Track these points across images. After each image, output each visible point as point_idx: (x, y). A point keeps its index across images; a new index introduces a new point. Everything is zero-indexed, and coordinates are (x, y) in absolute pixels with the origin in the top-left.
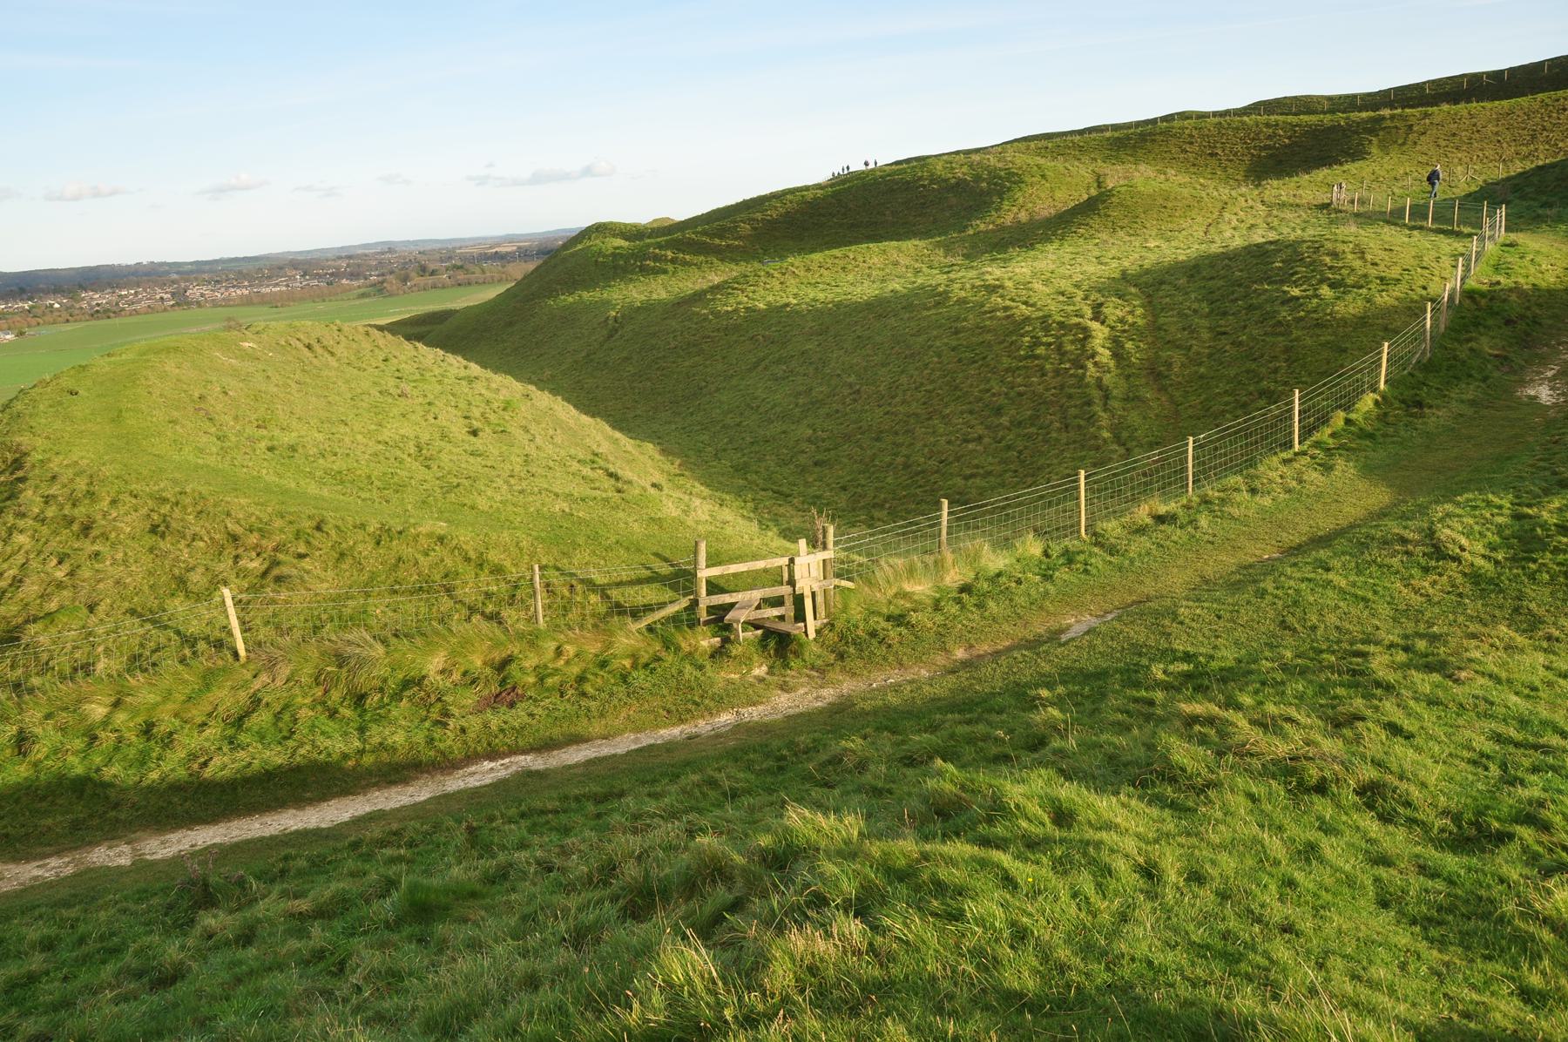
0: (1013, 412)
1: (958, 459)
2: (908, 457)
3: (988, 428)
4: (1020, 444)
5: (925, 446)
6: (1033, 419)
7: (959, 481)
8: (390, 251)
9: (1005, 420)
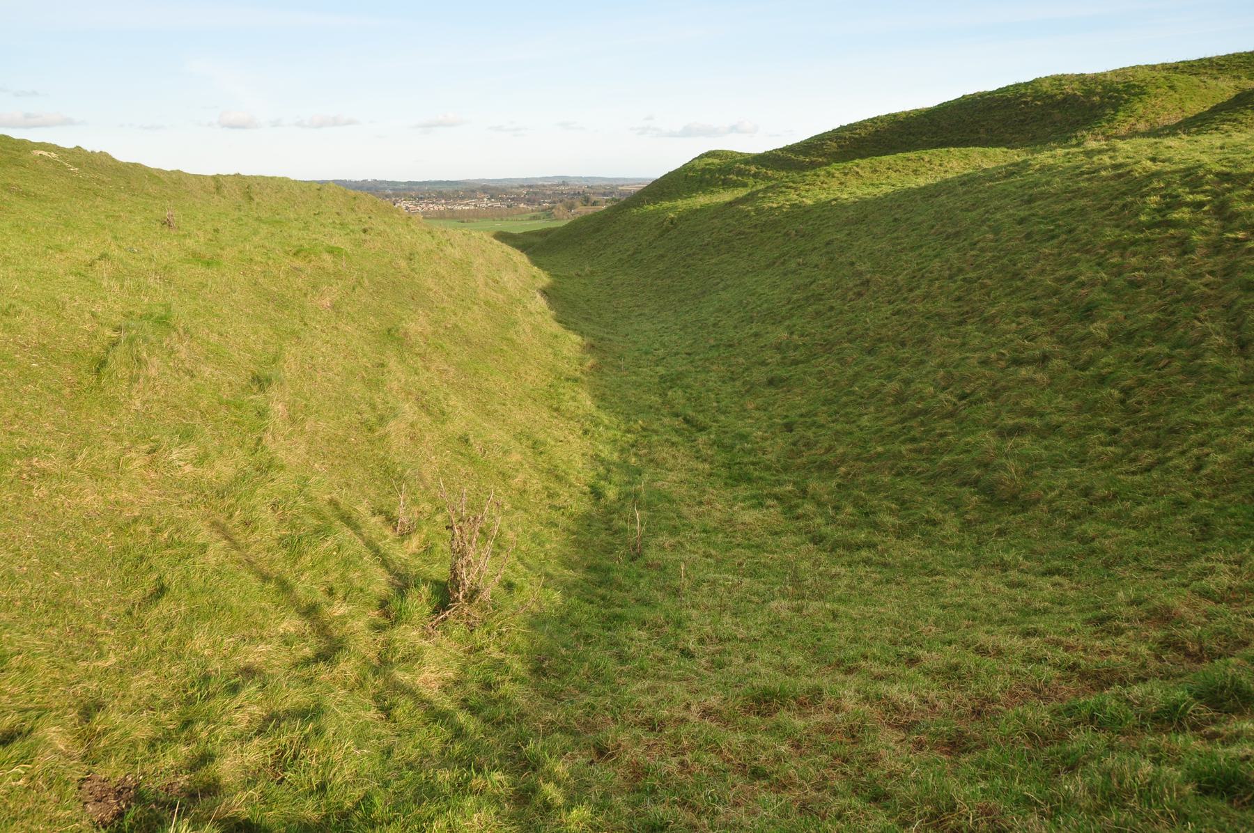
0: (1118, 314)
1: (994, 395)
2: (907, 382)
3: (1063, 341)
4: (1129, 375)
5: (942, 365)
6: (1160, 329)
7: (988, 439)
8: (564, 184)
9: (1099, 328)
